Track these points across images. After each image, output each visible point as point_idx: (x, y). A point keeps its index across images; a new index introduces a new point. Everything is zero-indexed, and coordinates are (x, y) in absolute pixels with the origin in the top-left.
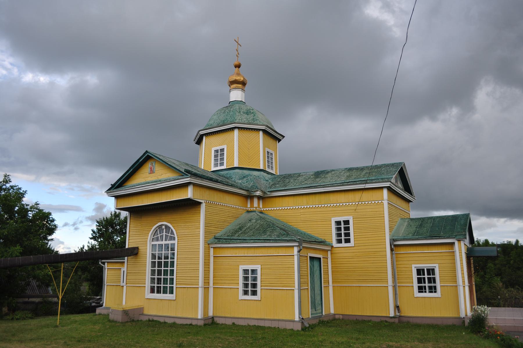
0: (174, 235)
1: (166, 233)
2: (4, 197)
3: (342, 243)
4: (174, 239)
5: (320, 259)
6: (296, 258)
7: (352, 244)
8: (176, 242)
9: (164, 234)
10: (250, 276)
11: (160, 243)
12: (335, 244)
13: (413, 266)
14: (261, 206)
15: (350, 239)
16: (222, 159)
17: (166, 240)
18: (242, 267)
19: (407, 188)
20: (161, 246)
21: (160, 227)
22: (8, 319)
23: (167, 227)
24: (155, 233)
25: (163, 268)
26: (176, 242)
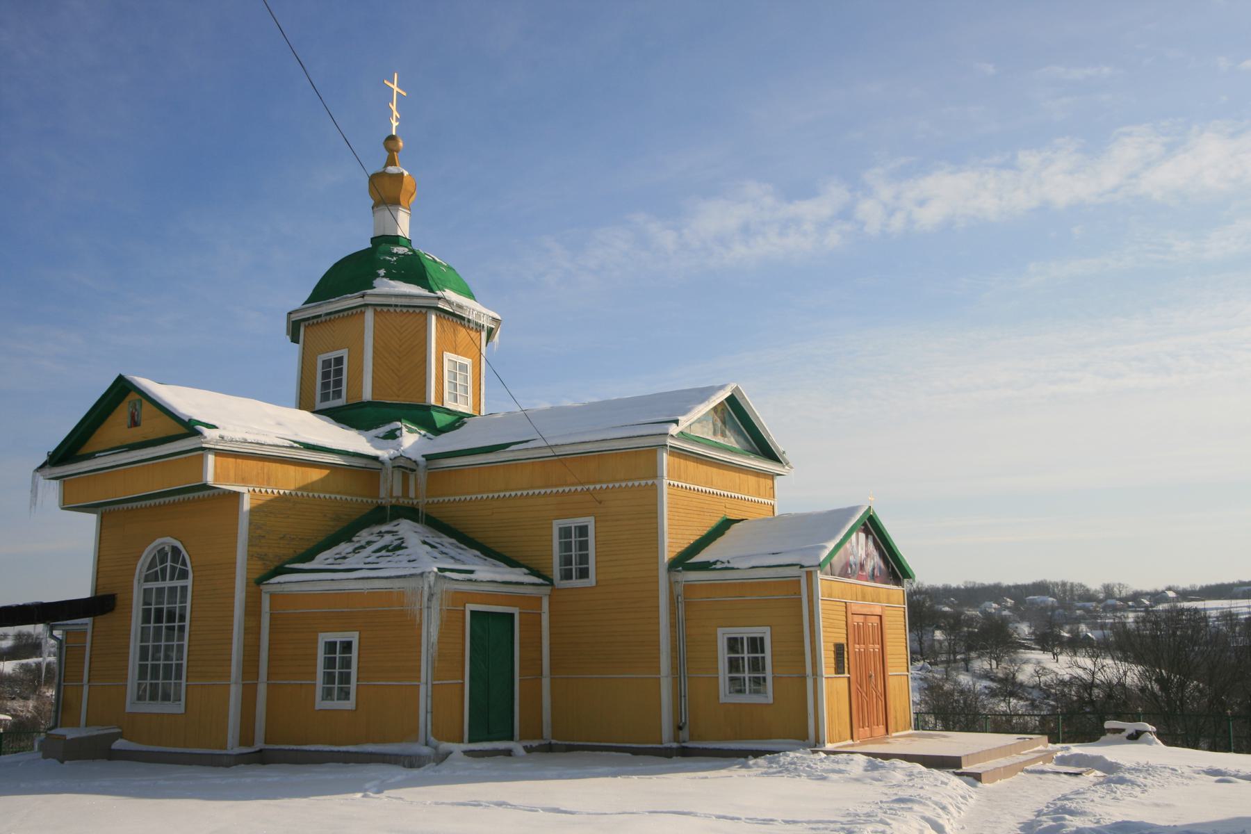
3: (78, 725)
4: (183, 575)
5: (512, 615)
6: (86, 689)
8: (189, 582)
12: (556, 575)
13: (720, 631)
17: (172, 578)
18: (324, 638)
20: (160, 591)
23: (176, 551)
24: (152, 565)
25: (163, 643)
26: (189, 582)
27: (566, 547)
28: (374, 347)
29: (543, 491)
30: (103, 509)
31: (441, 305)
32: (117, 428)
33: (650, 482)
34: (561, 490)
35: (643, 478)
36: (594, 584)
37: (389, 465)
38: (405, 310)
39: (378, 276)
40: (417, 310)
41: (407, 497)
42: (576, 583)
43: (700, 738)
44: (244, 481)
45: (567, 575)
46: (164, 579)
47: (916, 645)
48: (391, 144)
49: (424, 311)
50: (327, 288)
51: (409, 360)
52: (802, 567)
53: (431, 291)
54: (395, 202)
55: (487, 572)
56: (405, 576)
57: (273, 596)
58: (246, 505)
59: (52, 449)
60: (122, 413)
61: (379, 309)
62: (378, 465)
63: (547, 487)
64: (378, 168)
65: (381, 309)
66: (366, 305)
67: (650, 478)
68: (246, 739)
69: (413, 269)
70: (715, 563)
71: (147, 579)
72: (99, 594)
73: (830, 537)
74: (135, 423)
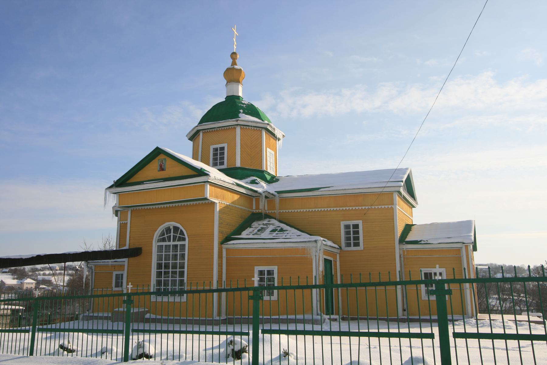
0: (184, 235)
1: (174, 233)
2: (54, 320)
4: (184, 239)
7: (361, 247)
8: (186, 243)
9: (172, 234)
10: (266, 276)
11: (167, 243)
14: (266, 208)
15: (359, 243)
16: (222, 158)
17: (174, 240)
19: (412, 194)
20: (168, 247)
21: (168, 230)
22: (6, 272)
23: (176, 229)
24: (163, 234)
26: (186, 243)
27: (348, 233)
28: (241, 144)
29: (335, 209)
30: (132, 208)
31: (268, 127)
32: (152, 170)
33: (390, 206)
34: (344, 209)
35: (386, 205)
36: (362, 249)
37: (264, 195)
38: (255, 128)
39: (240, 112)
40: (258, 129)
41: (259, 209)
42: (353, 248)
43: (413, 315)
44: (217, 197)
45: (348, 245)
46: (169, 241)
47: (526, 275)
48: (234, 56)
49: (260, 129)
50: (208, 117)
51: (255, 151)
52: (464, 243)
53: (263, 121)
54: (238, 81)
55: (330, 243)
56: (305, 242)
57: (227, 250)
58: (218, 208)
59: (116, 180)
60: (155, 164)
61: (242, 127)
62: (257, 195)
63: (337, 207)
64: (229, 66)
65: (244, 127)
66: (237, 125)
67: (390, 205)
68: (219, 314)
69: (252, 111)
70: (421, 241)
71: (159, 241)
72: (131, 247)
73: (470, 232)
74: (162, 169)
